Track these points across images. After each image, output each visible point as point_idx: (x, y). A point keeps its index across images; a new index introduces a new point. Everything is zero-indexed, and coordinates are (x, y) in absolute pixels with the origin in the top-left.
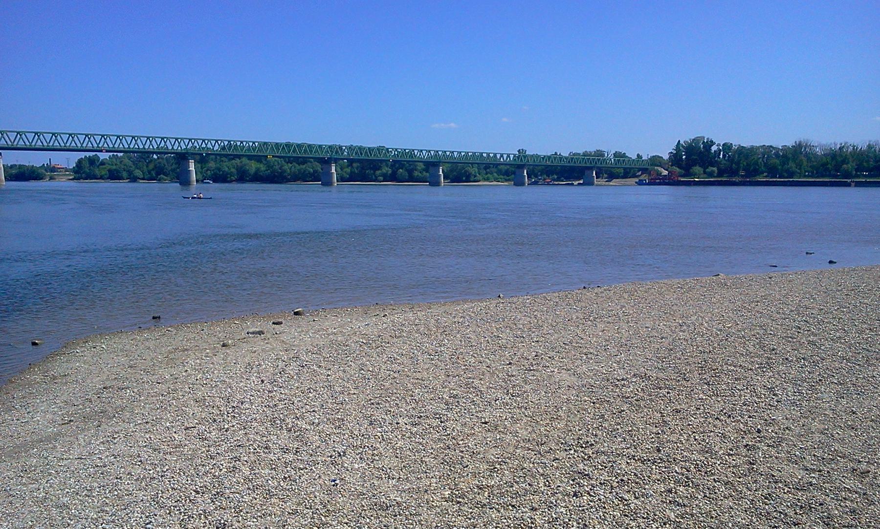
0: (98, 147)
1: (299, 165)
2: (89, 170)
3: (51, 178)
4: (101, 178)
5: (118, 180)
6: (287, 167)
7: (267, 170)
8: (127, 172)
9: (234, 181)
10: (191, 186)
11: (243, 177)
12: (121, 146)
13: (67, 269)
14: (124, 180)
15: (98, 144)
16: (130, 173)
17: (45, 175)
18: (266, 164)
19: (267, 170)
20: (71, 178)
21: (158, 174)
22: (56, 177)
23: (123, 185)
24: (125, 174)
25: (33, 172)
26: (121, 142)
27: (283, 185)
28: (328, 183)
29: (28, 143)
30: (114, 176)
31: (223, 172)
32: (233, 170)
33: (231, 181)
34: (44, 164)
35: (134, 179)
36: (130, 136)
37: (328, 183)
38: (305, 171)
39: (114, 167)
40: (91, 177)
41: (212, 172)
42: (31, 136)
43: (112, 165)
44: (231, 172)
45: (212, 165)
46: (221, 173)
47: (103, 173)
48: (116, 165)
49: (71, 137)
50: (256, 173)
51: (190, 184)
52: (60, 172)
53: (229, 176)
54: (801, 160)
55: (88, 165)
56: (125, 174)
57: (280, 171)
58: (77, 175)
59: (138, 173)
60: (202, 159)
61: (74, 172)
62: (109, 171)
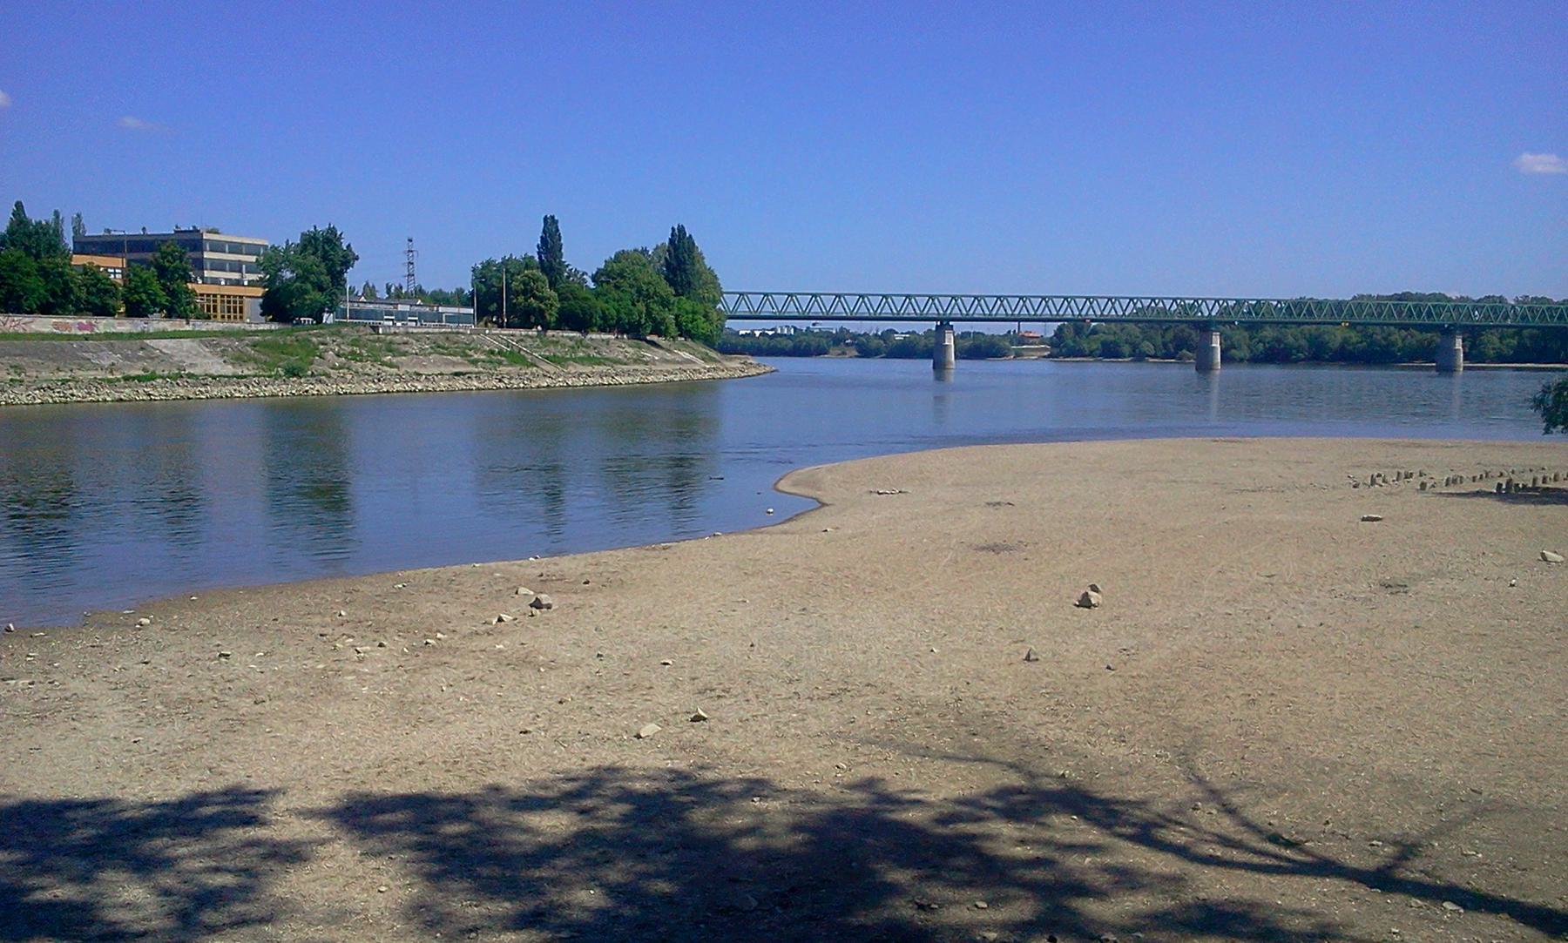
0: (1102, 314)
1: (1421, 333)
2: (1074, 341)
3: (1018, 355)
4: (1091, 354)
5: (1114, 357)
6: (1397, 337)
7: (1361, 342)
8: (1130, 344)
9: (1303, 360)
10: (1212, 372)
11: (1319, 354)
12: (1113, 313)
13: (447, 659)
14: (1125, 357)
15: (1124, 311)
16: (1134, 346)
17: (1009, 349)
18: (1361, 332)
19: (1361, 342)
20: (1046, 354)
21: (1178, 348)
22: (1024, 353)
23: (1122, 370)
24: (1126, 349)
25: (993, 345)
26: (1113, 307)
27: (1388, 372)
28: (1447, 369)
29: (987, 312)
30: (1110, 352)
31: (1286, 344)
32: (1303, 342)
33: (1297, 361)
34: (1009, 332)
35: (1139, 357)
36: (970, 296)
37: (1447, 369)
38: (1430, 344)
39: (1111, 338)
40: (525, 318)
41: (1267, 345)
42: (899, 301)
43: (1109, 334)
44: (1300, 346)
45: (1269, 333)
46: (1282, 346)
47: (1094, 347)
48: (1115, 333)
49: (976, 301)
50: (1342, 347)
51: (1212, 369)
52: (1031, 344)
53: (1294, 351)
54: (86, 270)
55: (1072, 334)
56: (1126, 349)
57: (1384, 343)
58: (1056, 351)
59: (1147, 347)
60: (1473, 334)
61: (1052, 345)
62: (1104, 344)
